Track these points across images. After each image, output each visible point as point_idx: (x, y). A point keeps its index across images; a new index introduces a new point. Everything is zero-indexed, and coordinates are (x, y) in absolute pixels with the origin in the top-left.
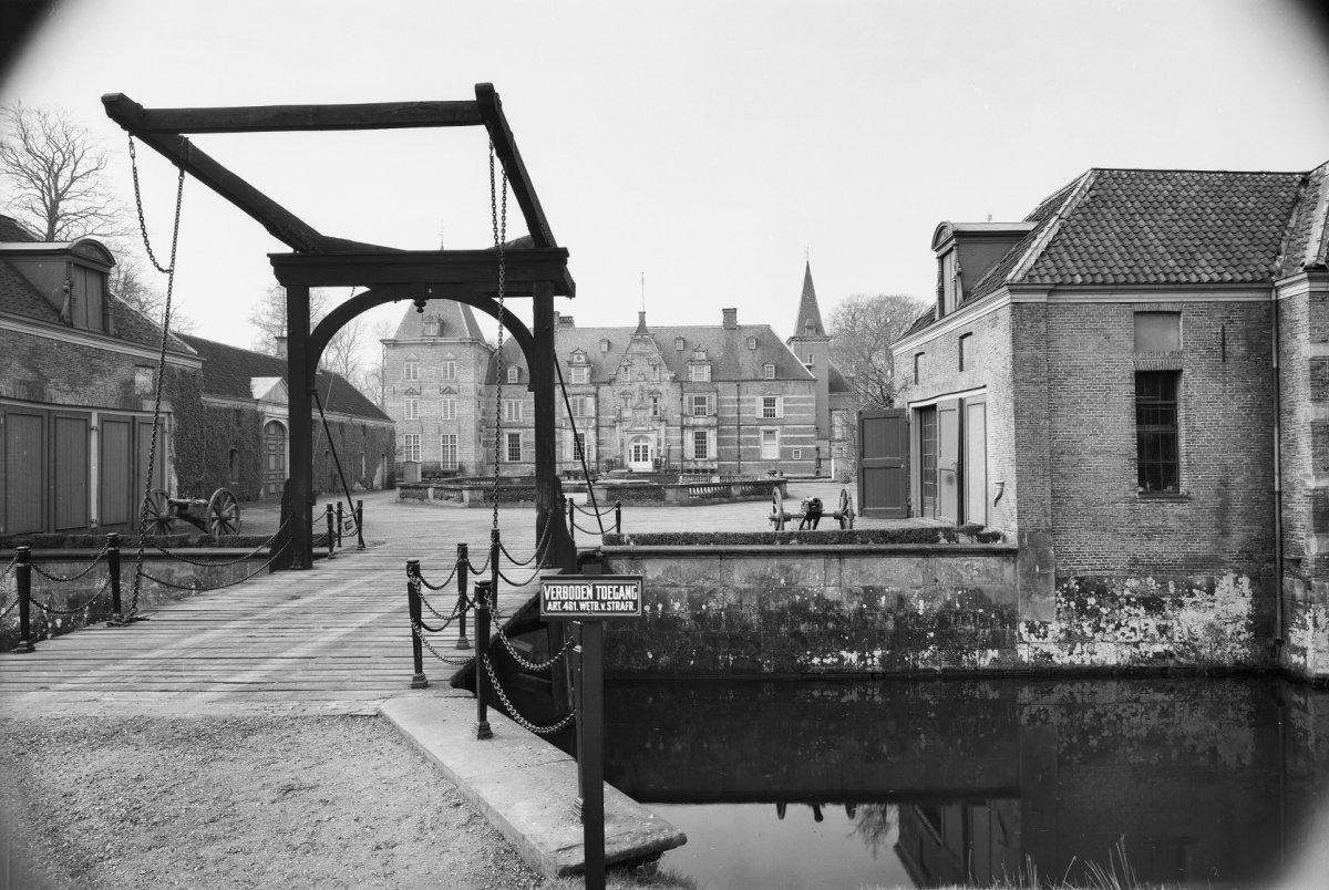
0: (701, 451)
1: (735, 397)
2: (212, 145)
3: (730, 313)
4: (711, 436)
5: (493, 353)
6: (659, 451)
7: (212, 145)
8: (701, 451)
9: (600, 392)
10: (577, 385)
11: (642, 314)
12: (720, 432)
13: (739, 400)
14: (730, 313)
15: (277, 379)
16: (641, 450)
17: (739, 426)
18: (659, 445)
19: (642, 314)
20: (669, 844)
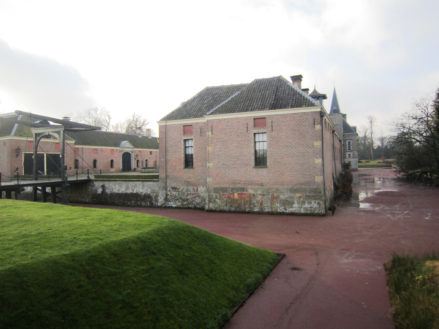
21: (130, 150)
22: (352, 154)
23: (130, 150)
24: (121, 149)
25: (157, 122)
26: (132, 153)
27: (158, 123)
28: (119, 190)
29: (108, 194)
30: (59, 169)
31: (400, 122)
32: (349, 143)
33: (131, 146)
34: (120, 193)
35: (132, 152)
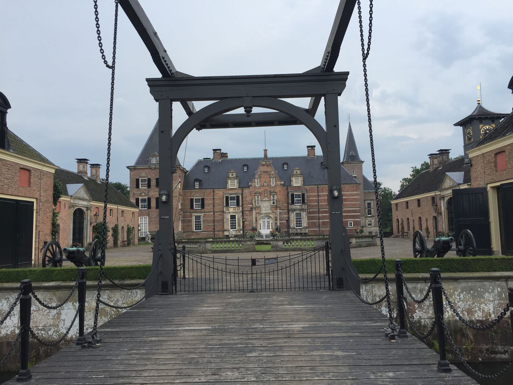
0: (299, 222)
1: (316, 194)
2: (110, 64)
3: (152, 248)
4: (304, 215)
5: (186, 173)
6: (276, 223)
7: (110, 64)
8: (299, 222)
9: (244, 193)
10: (232, 189)
11: (265, 151)
12: (309, 213)
13: (318, 195)
14: (152, 248)
15: (83, 184)
16: (266, 227)
17: (319, 209)
18: (276, 220)
19: (265, 151)
20: (450, 150)
21: (85, 203)
22: (374, 220)
23: (85, 203)
24: (72, 201)
25: (128, 167)
26: (87, 210)
27: (130, 169)
28: (470, 311)
29: (425, 326)
30: (438, 257)
31: (172, 299)
32: (198, 218)
33: (86, 196)
34: (479, 321)
35: (88, 209)
